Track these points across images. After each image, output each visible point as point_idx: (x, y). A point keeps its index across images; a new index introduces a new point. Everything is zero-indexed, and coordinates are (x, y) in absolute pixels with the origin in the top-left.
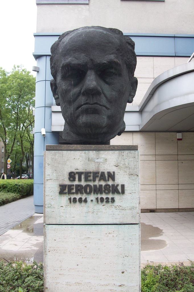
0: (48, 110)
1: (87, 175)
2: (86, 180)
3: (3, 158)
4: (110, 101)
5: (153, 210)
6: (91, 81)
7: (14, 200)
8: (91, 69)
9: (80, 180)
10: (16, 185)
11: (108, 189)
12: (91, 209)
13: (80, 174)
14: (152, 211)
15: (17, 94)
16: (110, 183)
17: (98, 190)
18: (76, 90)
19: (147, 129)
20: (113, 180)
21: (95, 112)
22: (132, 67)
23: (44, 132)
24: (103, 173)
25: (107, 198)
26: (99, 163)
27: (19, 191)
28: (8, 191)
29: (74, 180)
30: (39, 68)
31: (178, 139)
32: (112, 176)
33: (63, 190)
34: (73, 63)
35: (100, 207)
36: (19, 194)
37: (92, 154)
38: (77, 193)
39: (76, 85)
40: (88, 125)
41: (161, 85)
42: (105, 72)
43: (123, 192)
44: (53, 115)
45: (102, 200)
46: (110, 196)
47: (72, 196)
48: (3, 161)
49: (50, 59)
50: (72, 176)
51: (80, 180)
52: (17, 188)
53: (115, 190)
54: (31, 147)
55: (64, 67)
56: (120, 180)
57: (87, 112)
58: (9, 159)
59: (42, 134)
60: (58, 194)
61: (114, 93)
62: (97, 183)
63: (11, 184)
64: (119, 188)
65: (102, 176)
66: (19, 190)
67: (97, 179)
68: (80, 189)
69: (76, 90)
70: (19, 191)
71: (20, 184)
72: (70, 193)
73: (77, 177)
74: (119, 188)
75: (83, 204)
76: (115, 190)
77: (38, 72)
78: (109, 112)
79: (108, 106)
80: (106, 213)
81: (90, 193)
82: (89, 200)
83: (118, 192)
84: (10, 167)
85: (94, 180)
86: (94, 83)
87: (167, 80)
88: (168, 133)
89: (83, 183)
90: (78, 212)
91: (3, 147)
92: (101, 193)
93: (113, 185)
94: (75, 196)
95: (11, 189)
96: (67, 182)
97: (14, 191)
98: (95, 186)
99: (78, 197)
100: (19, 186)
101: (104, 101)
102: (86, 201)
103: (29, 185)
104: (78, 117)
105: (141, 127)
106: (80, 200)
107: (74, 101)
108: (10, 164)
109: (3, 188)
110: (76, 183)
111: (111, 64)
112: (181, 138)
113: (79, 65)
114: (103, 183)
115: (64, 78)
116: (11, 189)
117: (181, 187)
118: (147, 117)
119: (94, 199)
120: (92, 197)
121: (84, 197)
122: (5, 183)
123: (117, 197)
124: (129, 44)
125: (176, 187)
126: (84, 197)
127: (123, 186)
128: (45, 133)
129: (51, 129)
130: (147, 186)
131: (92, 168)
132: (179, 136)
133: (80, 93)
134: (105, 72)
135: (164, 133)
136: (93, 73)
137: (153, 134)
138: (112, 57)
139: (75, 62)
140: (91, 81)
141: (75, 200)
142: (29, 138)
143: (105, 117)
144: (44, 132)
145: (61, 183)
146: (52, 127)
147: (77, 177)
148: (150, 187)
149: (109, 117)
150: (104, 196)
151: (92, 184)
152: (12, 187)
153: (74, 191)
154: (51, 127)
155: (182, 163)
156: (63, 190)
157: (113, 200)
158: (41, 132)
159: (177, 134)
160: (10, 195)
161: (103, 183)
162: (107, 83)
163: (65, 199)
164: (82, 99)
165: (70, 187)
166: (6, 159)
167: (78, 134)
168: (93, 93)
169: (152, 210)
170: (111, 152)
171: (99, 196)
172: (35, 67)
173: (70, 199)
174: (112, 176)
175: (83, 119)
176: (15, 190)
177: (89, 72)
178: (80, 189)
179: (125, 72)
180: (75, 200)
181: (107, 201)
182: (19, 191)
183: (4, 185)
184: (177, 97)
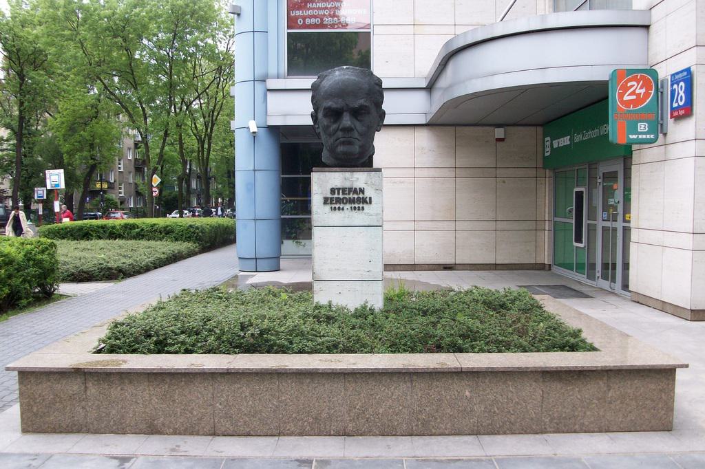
0: (259, 87)
1: (344, 190)
2: (343, 194)
3: (130, 173)
4: (361, 135)
5: (450, 266)
6: (347, 121)
7: (191, 254)
8: (346, 111)
9: (339, 194)
10: (191, 226)
11: (359, 200)
12: (347, 215)
13: (339, 189)
14: (447, 267)
15: (168, 30)
16: (361, 196)
17: (352, 201)
18: (335, 126)
19: (439, 121)
20: (364, 194)
21: (350, 143)
22: (379, 104)
23: (253, 128)
24: (356, 189)
25: (359, 207)
26: (353, 181)
27: (197, 239)
28: (177, 240)
29: (334, 194)
30: (240, 8)
31: (498, 140)
32: (362, 191)
33: (326, 201)
34: (333, 107)
35: (354, 213)
36: (198, 245)
37: (348, 174)
38: (336, 203)
39: (335, 122)
40: (345, 153)
41: (459, 51)
42: (357, 113)
43: (370, 203)
44: (270, 95)
45: (355, 208)
46: (361, 205)
47: (333, 206)
48: (131, 181)
49: (312, 97)
50: (333, 191)
51: (339, 194)
52: (194, 233)
53: (364, 201)
54: (199, 148)
55: (325, 109)
56: (367, 194)
57: (343, 143)
58: (155, 176)
59: (252, 131)
60: (19, 434)
61: (364, 128)
62: (351, 196)
63: (181, 224)
64: (368, 200)
65: (355, 191)
66: (196, 237)
67: (351, 193)
68: (338, 201)
69: (335, 126)
70: (198, 239)
71: (198, 224)
72: (331, 203)
73: (336, 191)
74: (368, 200)
75: (341, 211)
76: (364, 201)
77: (239, 15)
78: (360, 143)
79: (360, 139)
80: (358, 218)
81: (346, 203)
82: (345, 208)
83: (367, 203)
84: (157, 193)
85: (349, 194)
86: (349, 123)
87: (438, 73)
88: (480, 128)
89: (341, 196)
90: (337, 217)
91: (129, 149)
92: (354, 203)
93: (363, 198)
94: (335, 206)
95: (182, 235)
96: (329, 196)
97: (188, 239)
98: (350, 198)
99: (337, 206)
100: (197, 228)
101: (356, 135)
102: (343, 209)
103: (213, 228)
104: (337, 146)
105: (429, 117)
106: (339, 208)
107: (334, 134)
108: (157, 187)
109: (166, 234)
110: (336, 196)
111: (362, 107)
112: (503, 137)
113: (337, 108)
114: (356, 196)
115: (325, 116)
116: (182, 235)
117: (500, 225)
118: (439, 99)
119: (349, 208)
120: (348, 206)
121: (341, 206)
122: (168, 223)
123: (365, 206)
124: (377, 84)
125: (492, 225)
126: (341, 206)
127: (370, 198)
128: (256, 130)
129: (266, 122)
130: (440, 224)
131: (347, 185)
132: (499, 133)
133: (338, 129)
134: (357, 113)
135: (472, 128)
136: (348, 114)
137: (452, 129)
138: (362, 101)
139: (334, 106)
140: (347, 121)
141: (335, 209)
142: (193, 126)
143: (357, 147)
144: (253, 128)
145: (325, 196)
146: (268, 117)
147: (336, 191)
148: (446, 225)
149: (360, 147)
150: (357, 206)
151: (347, 196)
152: (182, 231)
153: (334, 202)
154: (266, 118)
155: (504, 182)
156: (326, 201)
157: (363, 208)
158: (248, 128)
159: (496, 129)
160: (183, 246)
161: (356, 196)
162: (357, 119)
163: (328, 207)
164: (340, 134)
165: (332, 199)
166: (150, 177)
167: (336, 159)
168: (348, 130)
169: (448, 266)
170: (361, 173)
171: (353, 206)
172: (234, 7)
173: (331, 208)
174: (362, 191)
175: (341, 149)
176: (189, 237)
177: (345, 113)
178: (338, 201)
179: (373, 110)
180: (335, 209)
181: (359, 209)
182: (197, 239)
183: (167, 227)
184: (478, 77)
